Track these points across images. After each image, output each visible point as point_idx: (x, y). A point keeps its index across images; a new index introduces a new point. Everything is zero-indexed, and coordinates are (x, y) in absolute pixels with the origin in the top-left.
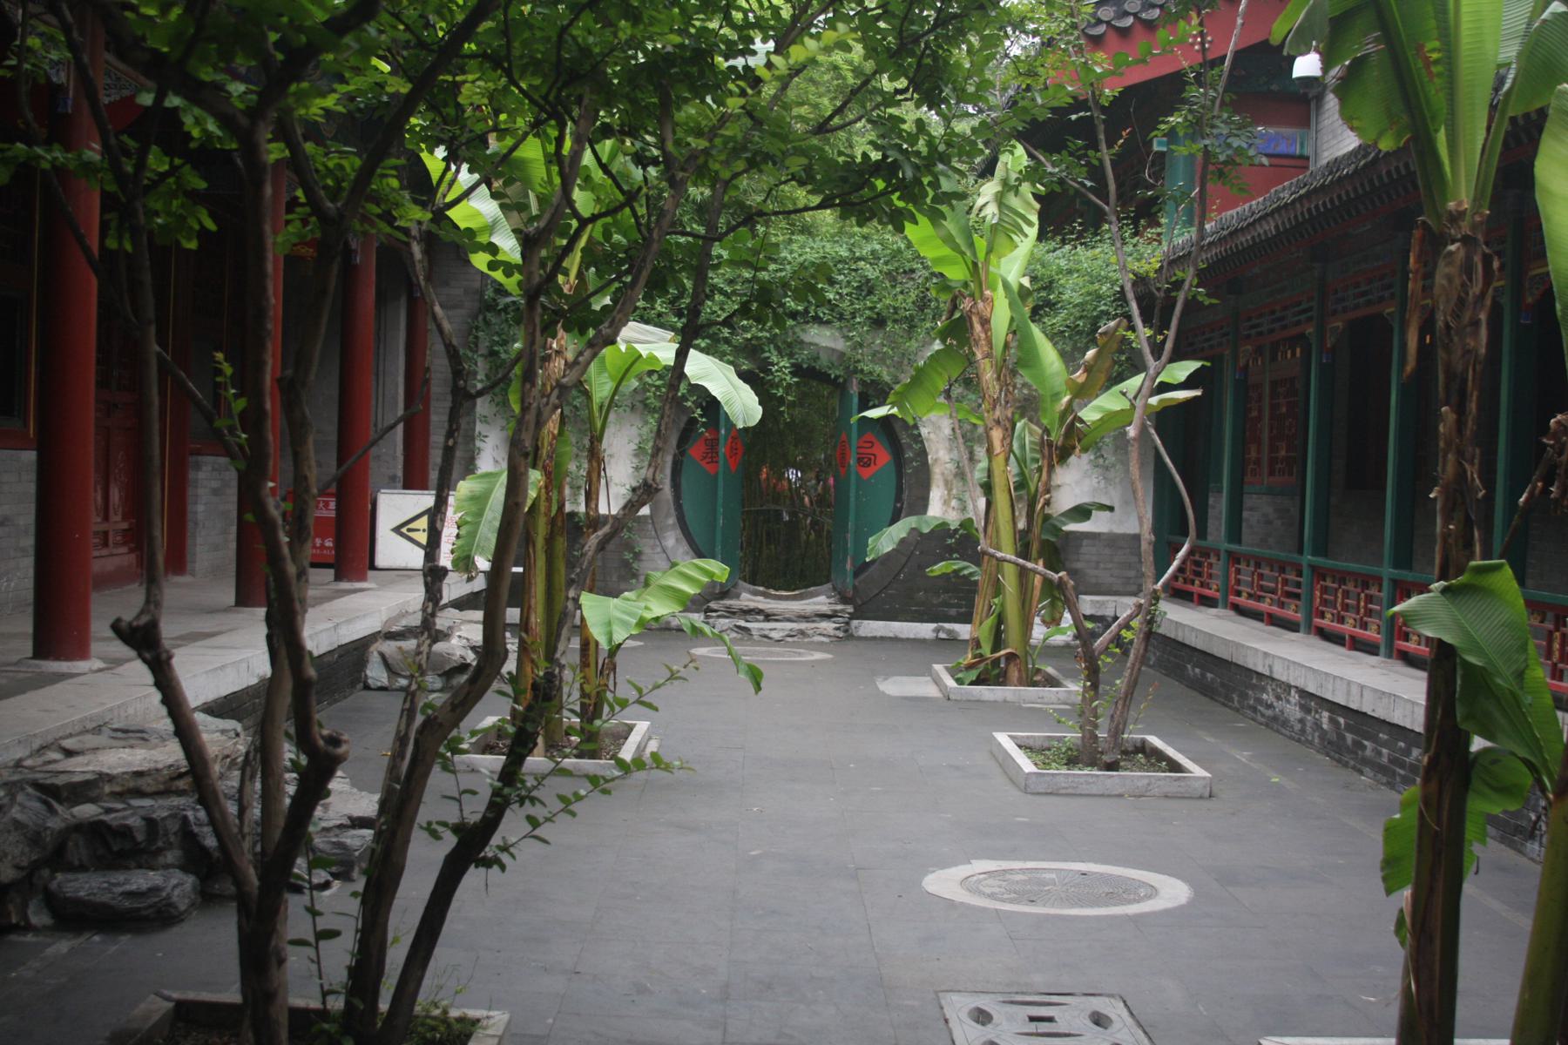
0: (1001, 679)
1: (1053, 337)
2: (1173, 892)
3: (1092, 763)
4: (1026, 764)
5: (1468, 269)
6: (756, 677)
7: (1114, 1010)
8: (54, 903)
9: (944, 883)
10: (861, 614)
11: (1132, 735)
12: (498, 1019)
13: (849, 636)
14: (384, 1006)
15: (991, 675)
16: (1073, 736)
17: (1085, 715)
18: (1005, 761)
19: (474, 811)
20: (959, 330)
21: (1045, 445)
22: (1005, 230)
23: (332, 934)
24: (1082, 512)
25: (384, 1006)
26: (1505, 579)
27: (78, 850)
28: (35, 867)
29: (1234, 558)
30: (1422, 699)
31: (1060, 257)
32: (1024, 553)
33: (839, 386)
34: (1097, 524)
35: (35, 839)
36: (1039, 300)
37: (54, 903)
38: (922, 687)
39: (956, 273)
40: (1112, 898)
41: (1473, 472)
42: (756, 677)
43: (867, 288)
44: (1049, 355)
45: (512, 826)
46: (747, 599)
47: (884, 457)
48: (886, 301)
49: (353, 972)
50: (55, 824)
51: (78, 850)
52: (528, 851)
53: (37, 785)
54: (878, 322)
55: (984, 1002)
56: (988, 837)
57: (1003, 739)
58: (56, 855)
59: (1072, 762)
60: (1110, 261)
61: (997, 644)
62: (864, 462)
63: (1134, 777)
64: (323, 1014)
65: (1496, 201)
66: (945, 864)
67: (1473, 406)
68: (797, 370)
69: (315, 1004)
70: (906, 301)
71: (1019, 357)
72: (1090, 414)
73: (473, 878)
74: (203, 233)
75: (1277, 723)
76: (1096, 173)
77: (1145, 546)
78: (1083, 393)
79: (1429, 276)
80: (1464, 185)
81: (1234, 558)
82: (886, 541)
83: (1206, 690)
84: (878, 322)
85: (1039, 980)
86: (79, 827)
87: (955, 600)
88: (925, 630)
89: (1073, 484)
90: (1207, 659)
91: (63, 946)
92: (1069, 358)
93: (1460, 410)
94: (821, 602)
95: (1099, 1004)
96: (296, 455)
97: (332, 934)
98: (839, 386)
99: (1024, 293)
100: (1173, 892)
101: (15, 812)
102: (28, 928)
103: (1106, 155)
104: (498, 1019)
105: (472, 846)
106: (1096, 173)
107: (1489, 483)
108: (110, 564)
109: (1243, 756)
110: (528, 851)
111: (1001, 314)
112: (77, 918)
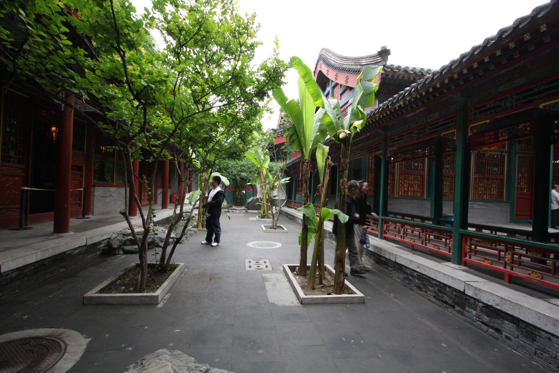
0: (264, 218)
1: (272, 174)
2: (279, 245)
3: (273, 228)
4: (264, 229)
5: (307, 166)
6: (229, 218)
7: (267, 261)
8: (123, 250)
9: (250, 244)
10: (248, 209)
11: (278, 225)
12: (182, 264)
13: (247, 212)
14: (165, 263)
15: (263, 217)
16: (271, 225)
17: (273, 222)
18: (262, 228)
19: (179, 236)
20: (259, 174)
21: (270, 188)
22: (265, 161)
23: (158, 253)
24: (275, 197)
25: (165, 263)
26: (312, 205)
27: (128, 243)
28: (120, 246)
29: (295, 202)
30: (469, 219)
31: (273, 164)
32: (267, 203)
33: (246, 180)
34: (277, 198)
35: (121, 241)
36: (270, 170)
37: (123, 250)
38: (254, 219)
39: (259, 166)
40: (271, 246)
41: (308, 192)
42: (229, 218)
43: (249, 168)
44: (271, 176)
45: (184, 238)
46: (234, 207)
47: (251, 189)
48: (251, 170)
49: (161, 259)
50: (124, 239)
51: (128, 243)
52: (186, 241)
53: (123, 234)
54: (251, 172)
55: (250, 260)
56: (258, 238)
57: (262, 226)
58: (125, 244)
59: (271, 228)
60: (281, 164)
61: (264, 213)
62: (249, 190)
63: (278, 230)
64: (156, 264)
65: (311, 158)
66: (251, 242)
67: (308, 184)
68: (240, 178)
69: (155, 263)
70: (254, 170)
71: (267, 177)
72: (276, 184)
73: (178, 245)
74: (142, 159)
75: (298, 223)
76: (274, 154)
77: (168, 201)
78: (275, 181)
79: (302, 167)
80: (307, 156)
81: (295, 202)
82: (250, 200)
83: (291, 219)
84: (251, 172)
85: (259, 257)
86: (129, 240)
87: (258, 208)
88: (257, 211)
89: (275, 193)
90: (291, 215)
91: (124, 256)
92: (273, 177)
93: (306, 184)
94: (243, 208)
95: (265, 260)
96: (422, 192)
97: (158, 253)
98: (246, 180)
99: (268, 169)
100: (279, 245)
101: (118, 238)
102: (119, 254)
103: (275, 152)
104: (182, 264)
105: (178, 241)
106: (274, 154)
107: (310, 193)
108: (145, 203)
109: (293, 227)
110: (186, 241)
111: (265, 172)
112: (126, 252)
